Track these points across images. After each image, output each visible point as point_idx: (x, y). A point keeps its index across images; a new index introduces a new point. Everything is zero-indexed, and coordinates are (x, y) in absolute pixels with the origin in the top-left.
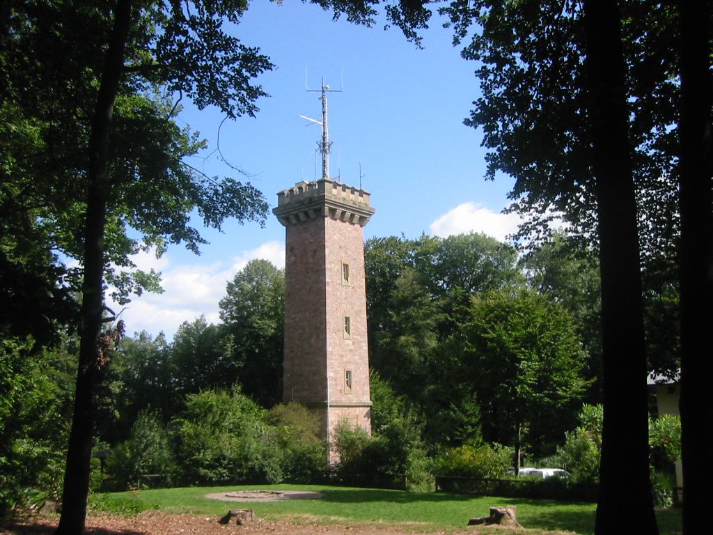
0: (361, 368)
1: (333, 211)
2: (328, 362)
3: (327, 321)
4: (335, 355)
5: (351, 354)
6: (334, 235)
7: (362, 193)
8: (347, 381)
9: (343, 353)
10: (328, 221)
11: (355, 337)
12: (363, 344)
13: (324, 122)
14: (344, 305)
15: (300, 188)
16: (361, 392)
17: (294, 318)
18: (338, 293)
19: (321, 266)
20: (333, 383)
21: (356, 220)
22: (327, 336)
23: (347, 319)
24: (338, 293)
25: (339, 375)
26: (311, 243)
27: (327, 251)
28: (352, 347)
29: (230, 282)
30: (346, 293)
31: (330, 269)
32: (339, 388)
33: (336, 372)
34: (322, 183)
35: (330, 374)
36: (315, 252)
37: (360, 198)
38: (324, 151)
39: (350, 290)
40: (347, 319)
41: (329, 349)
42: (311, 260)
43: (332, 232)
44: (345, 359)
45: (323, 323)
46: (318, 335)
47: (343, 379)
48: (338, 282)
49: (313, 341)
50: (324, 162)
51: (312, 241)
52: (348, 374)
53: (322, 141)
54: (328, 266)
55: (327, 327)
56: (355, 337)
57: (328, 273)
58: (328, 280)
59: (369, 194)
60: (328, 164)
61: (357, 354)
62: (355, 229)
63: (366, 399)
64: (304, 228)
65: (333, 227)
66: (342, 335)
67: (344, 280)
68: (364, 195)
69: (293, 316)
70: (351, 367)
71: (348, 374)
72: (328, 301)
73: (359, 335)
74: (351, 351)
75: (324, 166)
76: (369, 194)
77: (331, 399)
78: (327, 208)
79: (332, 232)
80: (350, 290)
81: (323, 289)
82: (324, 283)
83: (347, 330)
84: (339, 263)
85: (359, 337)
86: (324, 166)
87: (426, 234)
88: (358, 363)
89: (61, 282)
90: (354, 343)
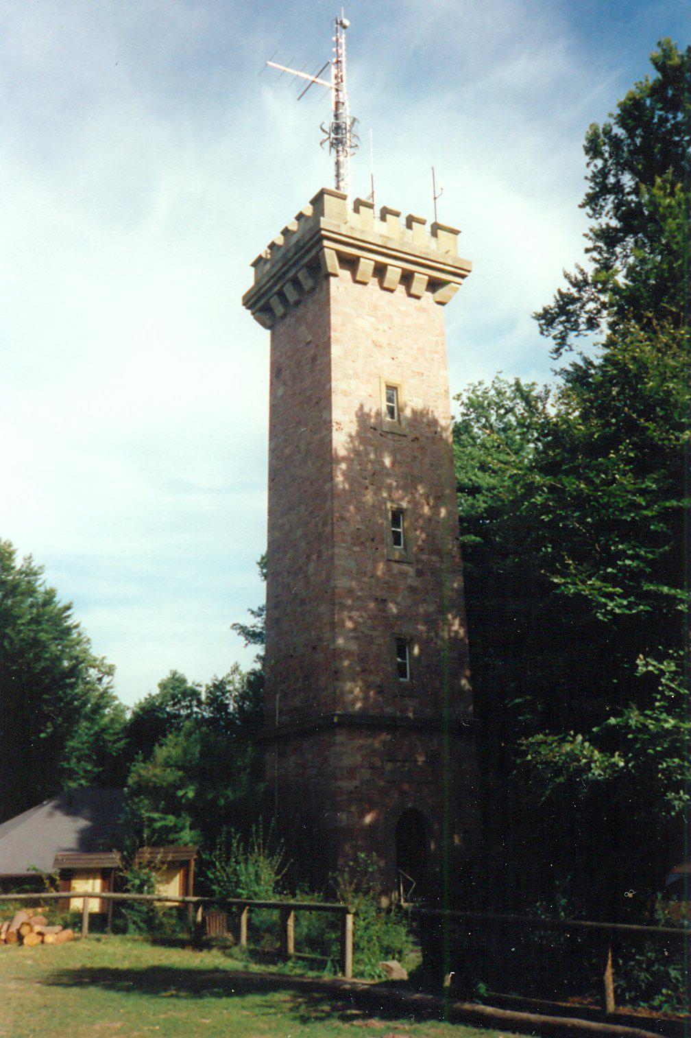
28: (417, 583)
36: (314, 359)
90: (419, 573)
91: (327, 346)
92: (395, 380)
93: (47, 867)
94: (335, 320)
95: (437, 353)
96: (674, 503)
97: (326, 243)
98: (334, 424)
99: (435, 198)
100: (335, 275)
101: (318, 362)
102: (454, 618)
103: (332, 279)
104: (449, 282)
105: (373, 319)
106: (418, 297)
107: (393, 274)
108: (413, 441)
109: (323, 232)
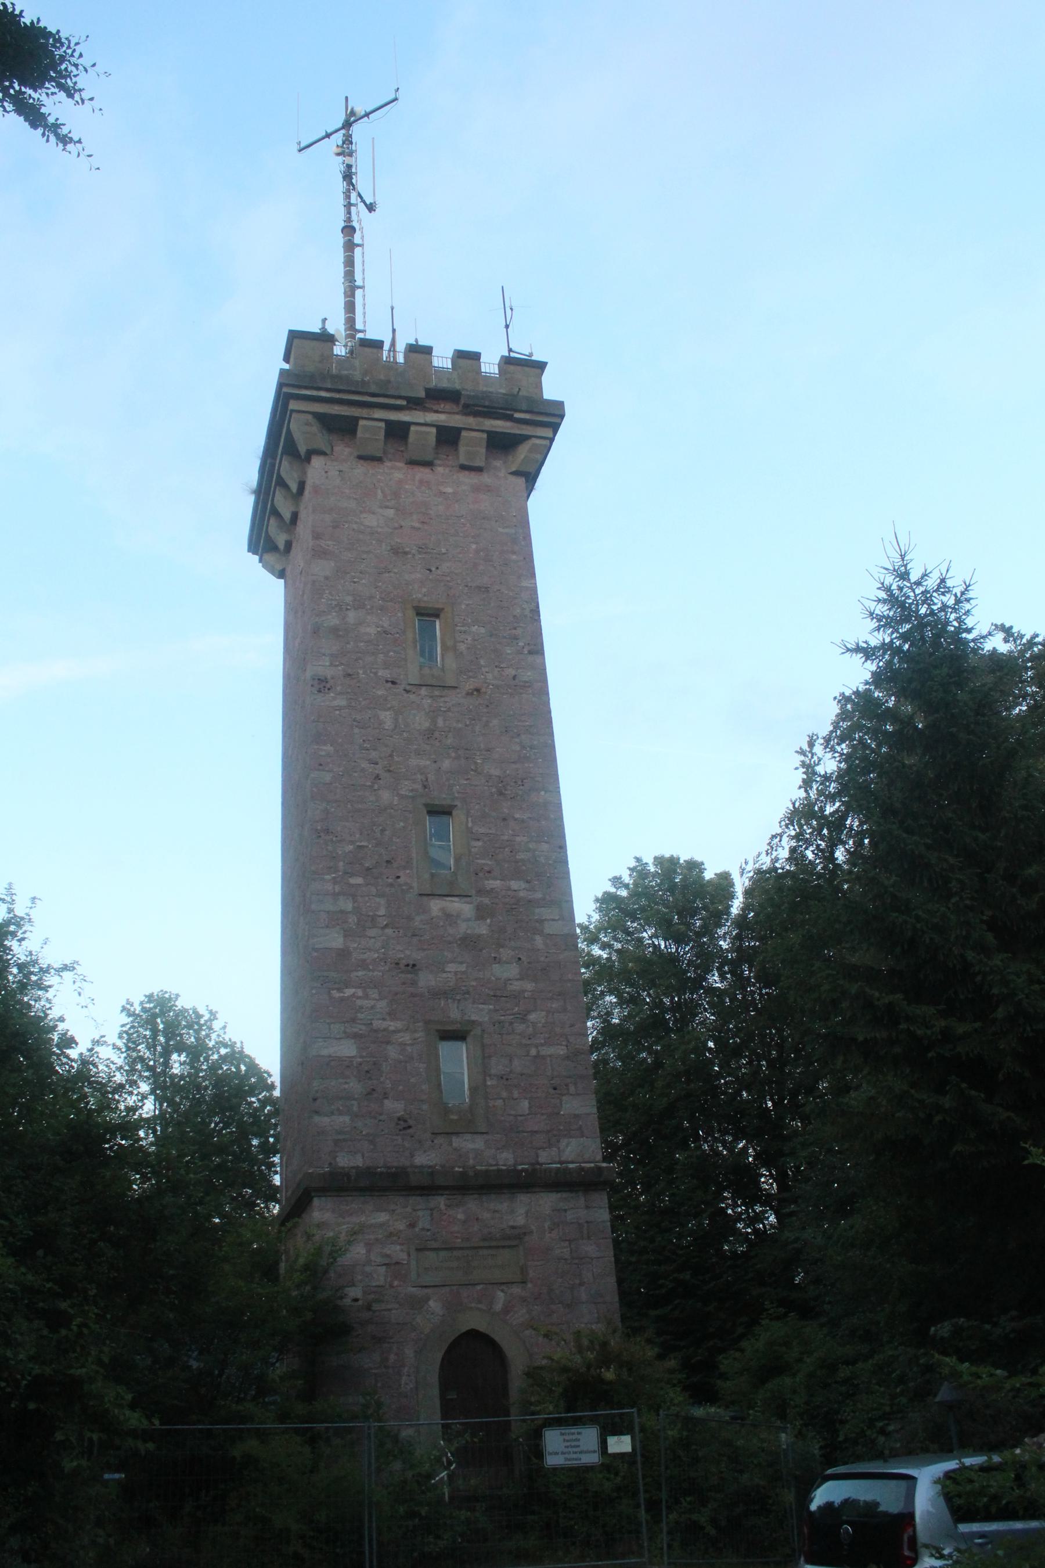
44: (426, 980)
90: (481, 913)
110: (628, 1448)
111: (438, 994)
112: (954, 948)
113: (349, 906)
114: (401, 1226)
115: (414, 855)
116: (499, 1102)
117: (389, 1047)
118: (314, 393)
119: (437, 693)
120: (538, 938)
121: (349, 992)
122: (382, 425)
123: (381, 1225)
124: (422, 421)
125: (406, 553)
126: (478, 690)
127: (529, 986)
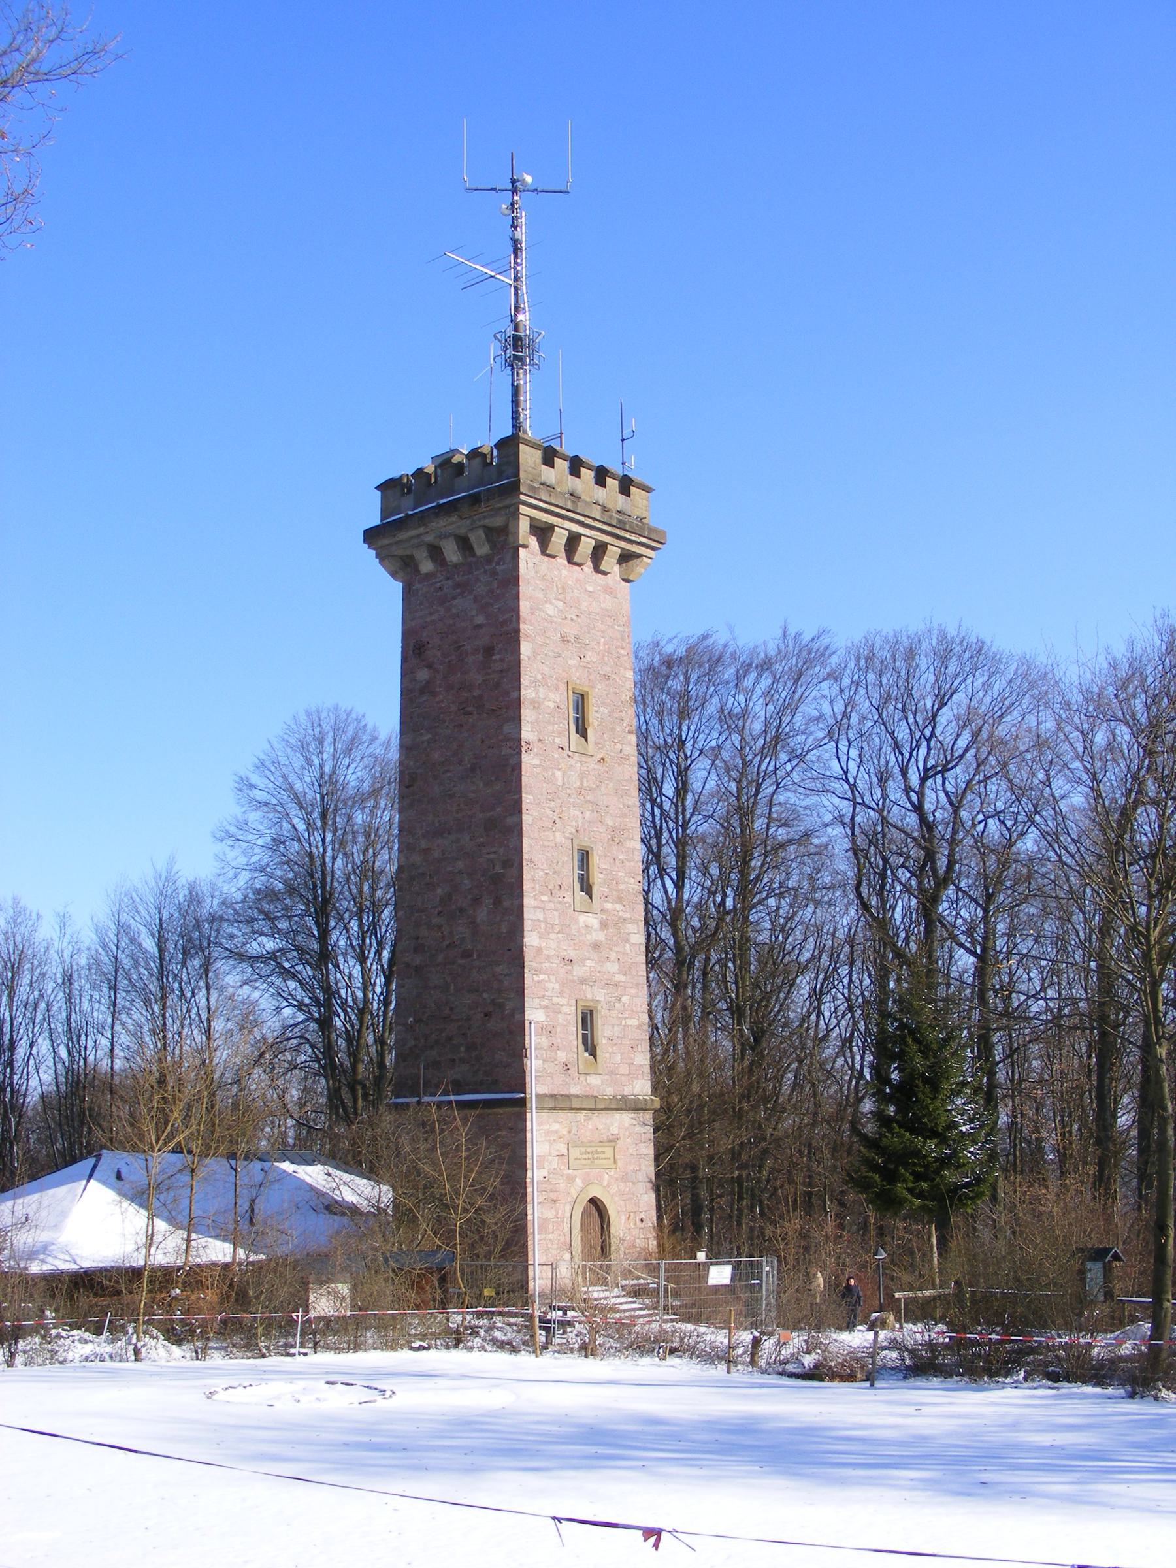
0: (624, 999)
1: (543, 532)
2: (530, 979)
3: (526, 856)
4: (548, 957)
5: (595, 956)
6: (548, 601)
7: (626, 483)
8: (584, 1036)
9: (572, 954)
10: (529, 558)
11: (609, 906)
12: (632, 928)
13: (516, 279)
14: (574, 812)
15: (349, 714)
16: (624, 1070)
17: (426, 851)
18: (558, 774)
19: (507, 693)
20: (545, 1042)
21: (610, 561)
22: (526, 901)
23: (584, 857)
24: (558, 774)
25: (561, 1019)
26: (479, 626)
27: (525, 649)
28: (601, 936)
29: (242, 773)
30: (582, 776)
31: (532, 702)
32: (562, 1056)
33: (552, 1009)
34: (509, 445)
35: (534, 1014)
36: (489, 651)
37: (621, 498)
38: (515, 363)
39: (592, 764)
40: (584, 857)
41: (531, 939)
42: (476, 678)
43: (540, 595)
44: (578, 971)
45: (514, 861)
46: (497, 902)
47: (572, 1032)
48: (557, 741)
49: (482, 915)
50: (516, 391)
51: (480, 619)
52: (587, 1019)
53: (510, 332)
54: (527, 692)
55: (526, 876)
56: (609, 906)
57: (527, 714)
58: (527, 733)
59: (647, 489)
60: (526, 397)
61: (613, 956)
62: (608, 590)
63: (642, 1087)
64: (458, 585)
65: (543, 578)
66: (569, 899)
67: (574, 736)
68: (633, 489)
69: (424, 844)
70: (598, 995)
71: (587, 1019)
72: (527, 798)
73: (620, 900)
74: (596, 946)
75: (515, 402)
76: (647, 489)
77: (536, 1087)
78: (524, 525)
79: (540, 595)
80: (592, 764)
81: (512, 761)
82: (515, 744)
83: (586, 886)
84: (563, 687)
85: (619, 907)
86: (515, 402)
87: (792, 631)
88: (616, 985)
89: (1168, 1301)
90: (604, 925)
91: (512, 638)
92: (583, 687)
93: (589, 1187)
94: (524, 606)
95: (623, 648)
96: (1166, 1084)
97: (523, 509)
98: (523, 744)
99: (623, 440)
100: (525, 546)
101: (496, 657)
102: (1163, 990)
103: (522, 551)
104: (639, 556)
105: (560, 604)
106: (605, 573)
107: (586, 547)
108: (599, 761)
109: (522, 497)
110: (726, 1281)
111: (583, 981)
112: (1035, 1047)
113: (541, 917)
114: (565, 1132)
115: (1170, 1104)
116: (608, 1055)
117: (560, 1016)
118: (581, 518)
119: (584, 759)
120: (627, 945)
121: (542, 977)
122: (567, 533)
123: (556, 1132)
124: (589, 534)
125: (568, 641)
126: (603, 759)
127: (623, 978)
